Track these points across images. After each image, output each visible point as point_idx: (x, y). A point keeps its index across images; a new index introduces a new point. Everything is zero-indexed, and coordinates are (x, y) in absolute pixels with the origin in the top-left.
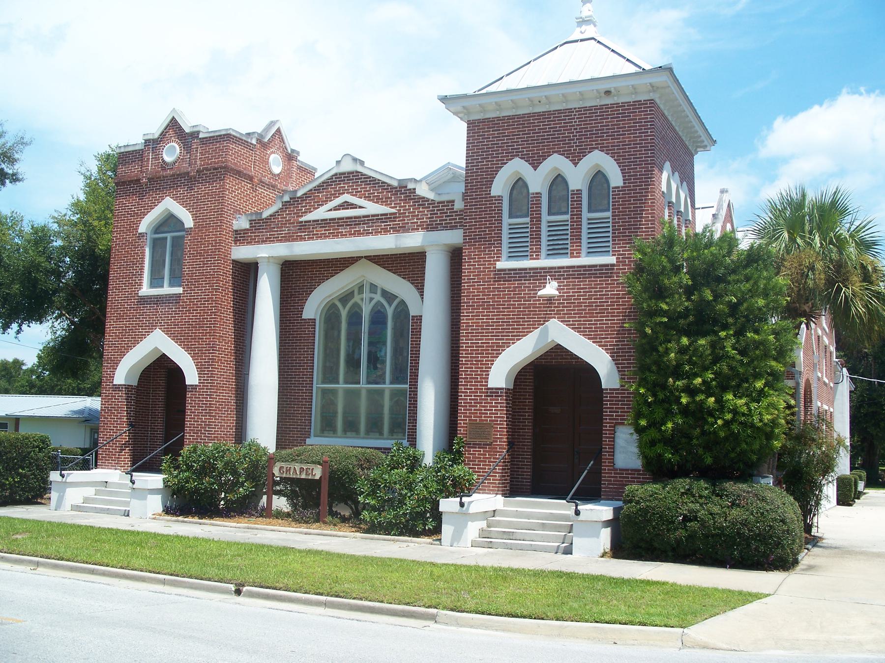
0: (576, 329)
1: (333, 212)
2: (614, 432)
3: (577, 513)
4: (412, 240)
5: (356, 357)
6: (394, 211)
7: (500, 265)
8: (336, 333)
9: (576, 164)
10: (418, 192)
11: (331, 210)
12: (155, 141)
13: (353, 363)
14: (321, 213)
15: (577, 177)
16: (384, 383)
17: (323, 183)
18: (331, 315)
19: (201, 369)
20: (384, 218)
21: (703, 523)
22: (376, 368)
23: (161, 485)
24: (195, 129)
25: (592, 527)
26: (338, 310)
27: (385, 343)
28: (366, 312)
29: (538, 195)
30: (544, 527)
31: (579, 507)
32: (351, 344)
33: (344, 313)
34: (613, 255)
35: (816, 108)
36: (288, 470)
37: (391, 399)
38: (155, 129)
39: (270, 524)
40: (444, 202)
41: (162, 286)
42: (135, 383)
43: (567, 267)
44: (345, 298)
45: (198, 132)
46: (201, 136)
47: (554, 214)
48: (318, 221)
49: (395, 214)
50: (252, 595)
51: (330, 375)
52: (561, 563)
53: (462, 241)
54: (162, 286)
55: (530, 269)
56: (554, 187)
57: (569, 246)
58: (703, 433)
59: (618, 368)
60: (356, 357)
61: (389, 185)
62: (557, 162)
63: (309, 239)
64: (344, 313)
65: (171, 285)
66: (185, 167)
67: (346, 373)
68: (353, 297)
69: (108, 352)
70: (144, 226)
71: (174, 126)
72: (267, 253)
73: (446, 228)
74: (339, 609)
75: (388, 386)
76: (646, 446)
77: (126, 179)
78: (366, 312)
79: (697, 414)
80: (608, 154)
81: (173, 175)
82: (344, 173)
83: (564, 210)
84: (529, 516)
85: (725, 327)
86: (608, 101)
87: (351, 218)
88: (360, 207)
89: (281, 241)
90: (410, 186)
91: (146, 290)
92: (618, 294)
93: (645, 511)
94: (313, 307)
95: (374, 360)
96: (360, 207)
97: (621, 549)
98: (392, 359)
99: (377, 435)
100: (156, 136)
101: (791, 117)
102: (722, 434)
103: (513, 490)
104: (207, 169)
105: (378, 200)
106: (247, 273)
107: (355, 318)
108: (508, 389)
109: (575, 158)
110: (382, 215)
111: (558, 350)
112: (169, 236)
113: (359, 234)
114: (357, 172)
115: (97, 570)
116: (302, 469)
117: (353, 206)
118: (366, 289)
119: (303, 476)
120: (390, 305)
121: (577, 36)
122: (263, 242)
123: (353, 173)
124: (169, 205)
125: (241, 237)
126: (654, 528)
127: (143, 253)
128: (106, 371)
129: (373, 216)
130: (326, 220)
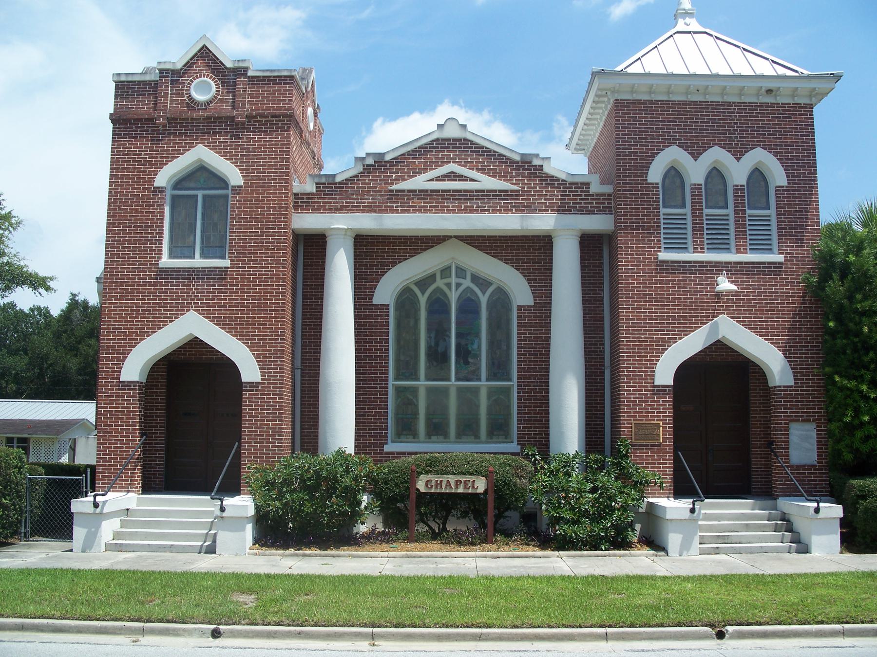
0: (748, 326)
1: (434, 182)
2: (787, 429)
3: (222, 509)
4: (543, 222)
6: (515, 187)
8: (412, 322)
9: (738, 159)
10: (546, 169)
11: (432, 180)
12: (174, 72)
15: (738, 172)
16: (479, 380)
17: (419, 147)
18: (406, 300)
19: (263, 363)
22: (467, 363)
23: (251, 511)
24: (241, 65)
25: (236, 523)
27: (478, 335)
28: (453, 297)
30: (747, 528)
31: (224, 503)
32: (433, 335)
33: (423, 300)
36: (439, 484)
38: (177, 58)
39: (423, 550)
40: (577, 184)
41: (194, 258)
42: (144, 381)
43: (735, 263)
44: (424, 283)
45: (246, 69)
46: (250, 73)
48: (415, 191)
51: (407, 370)
52: (205, 564)
54: (194, 258)
56: (709, 180)
57: (706, 242)
59: (790, 365)
60: (440, 349)
62: (716, 155)
63: (403, 211)
64: (423, 300)
65: (203, 255)
66: (226, 109)
67: (428, 368)
68: (435, 281)
70: (164, 177)
72: (341, 224)
73: (580, 212)
74: (862, 636)
76: (828, 441)
77: (130, 116)
78: (453, 297)
80: (771, 152)
81: (208, 118)
82: (449, 140)
86: (769, 100)
88: (472, 180)
89: (363, 211)
90: (536, 162)
91: (166, 261)
92: (789, 292)
94: (386, 292)
95: (464, 354)
96: (472, 180)
98: (488, 351)
100: (179, 66)
101: (389, 121)
103: (147, 488)
104: (262, 116)
106: (313, 249)
107: (438, 306)
108: (141, 383)
109: (738, 153)
110: (500, 191)
111: (195, 344)
112: (200, 194)
113: (472, 210)
114: (465, 140)
116: (458, 483)
119: (461, 490)
120: (423, 294)
122: (337, 210)
123: (460, 140)
124: (202, 153)
125: (303, 202)
127: (162, 212)
128: (105, 364)
129: (488, 191)
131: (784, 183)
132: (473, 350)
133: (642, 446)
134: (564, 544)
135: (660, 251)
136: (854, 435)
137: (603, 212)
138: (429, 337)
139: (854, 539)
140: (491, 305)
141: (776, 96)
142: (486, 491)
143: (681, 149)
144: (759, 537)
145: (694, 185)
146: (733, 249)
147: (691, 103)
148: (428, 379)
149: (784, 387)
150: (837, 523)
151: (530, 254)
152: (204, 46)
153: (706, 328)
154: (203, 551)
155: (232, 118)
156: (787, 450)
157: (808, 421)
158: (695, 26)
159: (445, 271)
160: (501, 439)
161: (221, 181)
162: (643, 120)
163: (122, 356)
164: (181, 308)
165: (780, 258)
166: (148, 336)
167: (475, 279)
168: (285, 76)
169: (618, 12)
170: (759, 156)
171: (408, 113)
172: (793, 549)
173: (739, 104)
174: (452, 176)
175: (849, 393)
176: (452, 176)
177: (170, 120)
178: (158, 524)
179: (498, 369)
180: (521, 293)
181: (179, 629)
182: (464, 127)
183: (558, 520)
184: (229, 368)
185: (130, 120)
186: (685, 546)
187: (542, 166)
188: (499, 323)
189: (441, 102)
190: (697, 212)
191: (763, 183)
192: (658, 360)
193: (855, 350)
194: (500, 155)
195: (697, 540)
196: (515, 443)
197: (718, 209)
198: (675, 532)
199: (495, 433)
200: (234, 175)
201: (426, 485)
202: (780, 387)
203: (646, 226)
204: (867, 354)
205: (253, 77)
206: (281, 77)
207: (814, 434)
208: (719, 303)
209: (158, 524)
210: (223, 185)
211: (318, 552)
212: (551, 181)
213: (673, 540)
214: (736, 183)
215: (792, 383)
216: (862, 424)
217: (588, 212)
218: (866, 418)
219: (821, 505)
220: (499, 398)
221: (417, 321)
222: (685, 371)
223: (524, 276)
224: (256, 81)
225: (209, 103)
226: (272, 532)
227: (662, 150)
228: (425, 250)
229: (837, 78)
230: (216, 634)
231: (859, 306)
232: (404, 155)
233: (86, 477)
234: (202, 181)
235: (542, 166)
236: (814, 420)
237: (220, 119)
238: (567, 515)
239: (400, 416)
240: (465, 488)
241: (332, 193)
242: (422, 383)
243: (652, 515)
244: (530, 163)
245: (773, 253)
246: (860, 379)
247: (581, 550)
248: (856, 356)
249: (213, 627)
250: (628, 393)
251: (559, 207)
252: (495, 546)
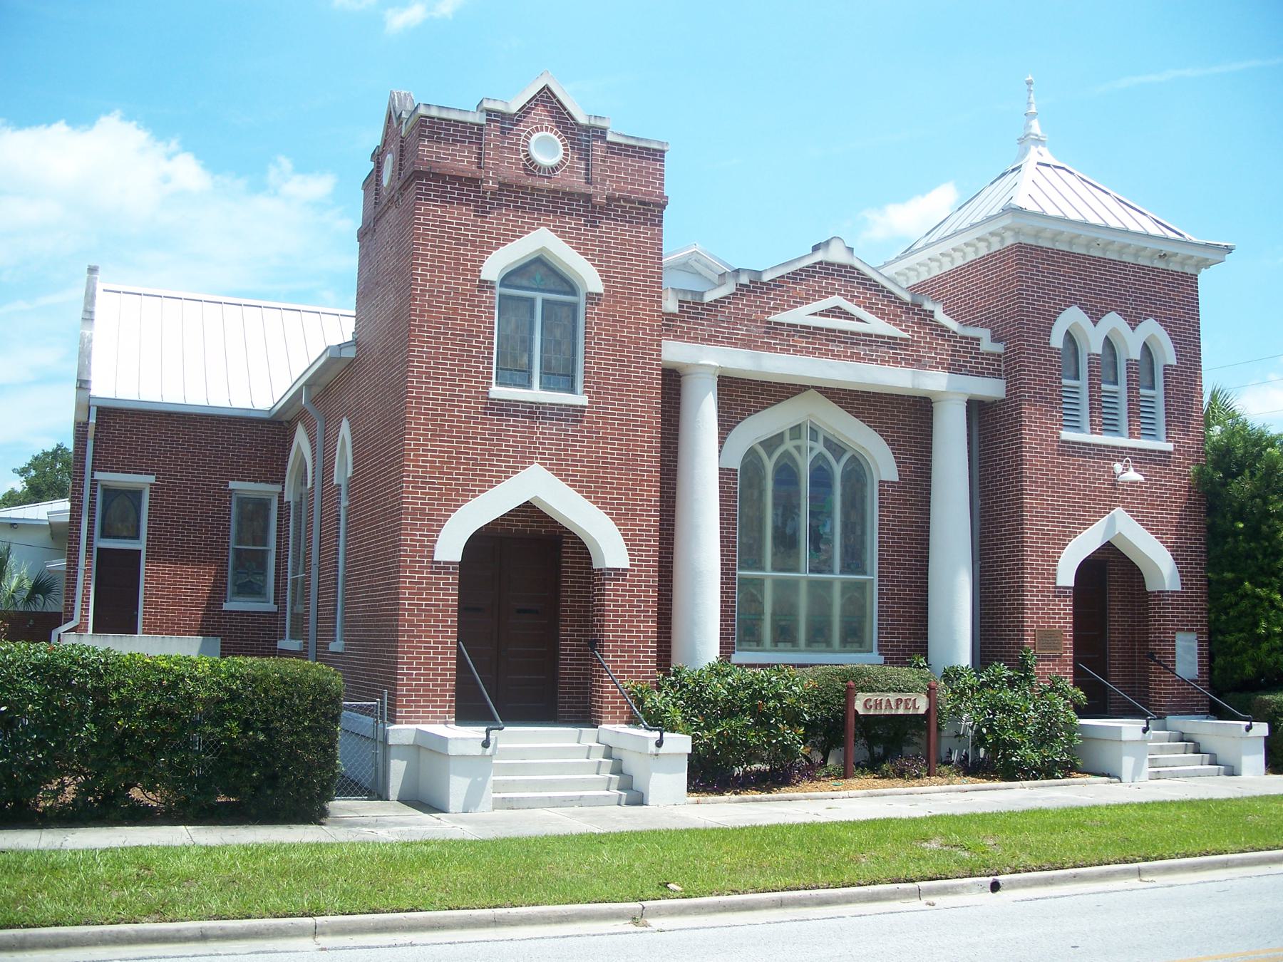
1: (818, 318)
4: (934, 381)
5: (788, 531)
6: (905, 335)
7: (1067, 435)
11: (815, 314)
13: (786, 542)
14: (800, 315)
15: (1131, 344)
16: (831, 572)
20: (891, 342)
24: (599, 123)
26: (760, 459)
28: (805, 467)
32: (780, 512)
33: (770, 465)
35: (60, 128)
36: (878, 704)
37: (843, 594)
41: (529, 385)
44: (771, 444)
45: (604, 131)
46: (610, 138)
48: (796, 326)
49: (907, 340)
50: (1013, 885)
62: (1113, 322)
64: (770, 465)
65: (545, 386)
66: (577, 182)
69: (412, 497)
70: (494, 266)
71: (546, 98)
72: (705, 359)
75: (837, 576)
76: (1211, 656)
77: (444, 171)
78: (805, 467)
82: (833, 264)
87: (846, 332)
92: (1177, 483)
95: (817, 538)
97: (708, 774)
99: (823, 646)
103: (468, 712)
104: (627, 200)
105: (883, 315)
107: (787, 474)
109: (1134, 323)
110: (889, 338)
112: (539, 297)
113: (858, 358)
114: (852, 267)
115: (1232, 861)
117: (849, 316)
118: (806, 433)
119: (901, 711)
120: (838, 462)
123: (845, 267)
124: (542, 240)
125: (670, 326)
128: (410, 535)
129: (877, 336)
130: (809, 327)
131: (1172, 359)
138: (775, 515)
139: (1280, 759)
140: (846, 476)
142: (928, 711)
146: (1126, 432)
148: (775, 569)
150: (1263, 741)
151: (908, 419)
152: (546, 88)
154: (623, 802)
155: (588, 198)
157: (1190, 630)
159: (796, 431)
160: (856, 647)
161: (567, 284)
163: (436, 525)
164: (520, 461)
165: (1169, 447)
166: (474, 496)
167: (829, 443)
168: (654, 150)
169: (401, 20)
170: (1151, 328)
171: (50, 122)
174: (837, 312)
176: (837, 312)
177: (504, 186)
178: (525, 768)
179: (854, 561)
180: (883, 464)
181: (958, 886)
182: (851, 250)
185: (444, 176)
186: (1137, 771)
188: (854, 502)
189: (108, 112)
195: (1146, 763)
196: (876, 652)
198: (459, 775)
200: (590, 278)
201: (865, 705)
203: (1054, 400)
205: (612, 143)
206: (648, 149)
207: (1195, 645)
208: (1115, 494)
209: (525, 768)
210: (568, 289)
211: (758, 796)
213: (457, 788)
215: (1179, 589)
219: (666, 735)
220: (855, 594)
221: (762, 492)
222: (480, 543)
224: (616, 149)
225: (554, 169)
226: (708, 774)
228: (779, 401)
229: (1229, 250)
230: (995, 887)
232: (782, 277)
233: (382, 703)
234: (538, 277)
237: (570, 195)
240: (906, 708)
241: (697, 317)
242: (804, 575)
243: (428, 752)
245: (1083, 432)
249: (991, 879)
250: (1032, 595)
252: (946, 781)
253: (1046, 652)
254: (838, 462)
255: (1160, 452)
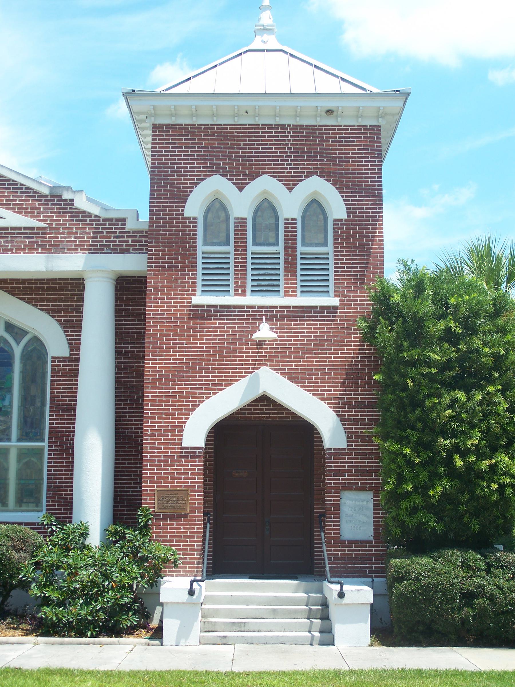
2: (338, 499)
4: (69, 263)
6: (42, 224)
9: (290, 189)
15: (291, 204)
16: (9, 440)
21: (492, 598)
27: (10, 390)
29: (242, 222)
30: (275, 613)
34: (336, 296)
37: (19, 460)
40: (111, 220)
43: (281, 307)
47: (259, 244)
53: (146, 269)
55: (234, 307)
56: (259, 213)
58: (473, 497)
59: (343, 424)
61: (36, 192)
62: (266, 185)
73: (114, 251)
79: (469, 477)
80: (329, 181)
83: (272, 240)
84: (247, 601)
85: (491, 381)
86: (330, 121)
90: (67, 196)
92: (343, 341)
93: (426, 588)
97: (387, 630)
98: (20, 408)
102: (494, 498)
105: (20, 210)
109: (291, 182)
110: (25, 228)
111: (264, 402)
120: (18, 343)
121: (257, 44)
126: (437, 608)
129: (13, 229)
131: (343, 215)
132: (4, 406)
133: (165, 517)
134: (47, 629)
135: (195, 294)
136: (399, 507)
137: (140, 251)
140: (26, 356)
141: (337, 117)
143: (224, 179)
144: (282, 625)
145: (238, 219)
147: (238, 126)
149: (335, 449)
151: (62, 297)
153: (244, 382)
156: (338, 523)
158: (272, 42)
160: (32, 506)
162: (186, 146)
165: (335, 302)
170: (315, 186)
172: (316, 641)
173: (294, 127)
175: (393, 456)
183: (46, 601)
184: (306, 431)
186: (184, 633)
187: (73, 200)
190: (241, 249)
191: (321, 217)
192: (187, 419)
193: (402, 407)
194: (28, 188)
195: (197, 626)
196: (44, 512)
197: (267, 248)
199: (25, 500)
202: (331, 449)
204: (414, 411)
207: (371, 505)
208: (260, 354)
212: (83, 216)
214: (287, 217)
216: (407, 494)
217: (123, 251)
218: (410, 488)
222: (220, 432)
223: (61, 324)
227: (203, 180)
231: (405, 354)
235: (73, 200)
236: (370, 489)
238: (55, 595)
239: (22, 482)
244: (60, 196)
246: (403, 441)
247: (64, 636)
248: (402, 413)
251: (91, 246)
253: (169, 512)
254: (18, 343)
255: (321, 307)
